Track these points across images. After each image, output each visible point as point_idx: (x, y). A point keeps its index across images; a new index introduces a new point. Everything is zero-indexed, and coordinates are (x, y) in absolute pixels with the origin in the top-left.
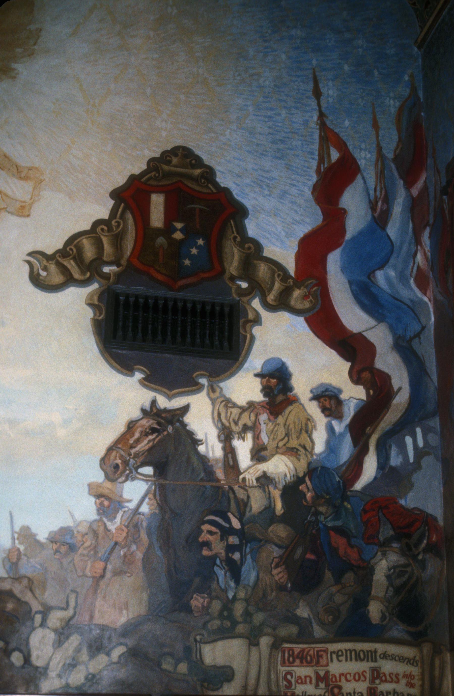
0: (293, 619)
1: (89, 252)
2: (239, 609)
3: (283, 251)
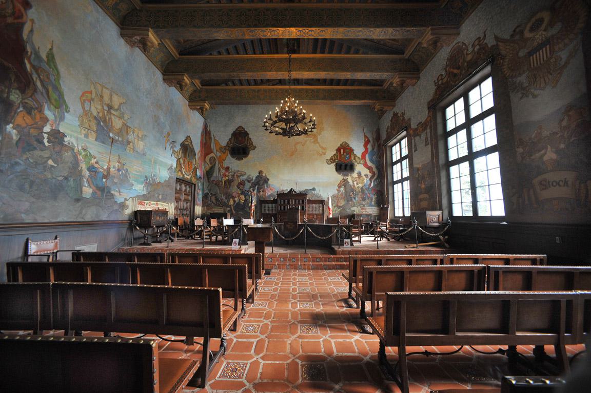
0: (362, 204)
1: (334, 159)
2: (355, 203)
3: (359, 155)
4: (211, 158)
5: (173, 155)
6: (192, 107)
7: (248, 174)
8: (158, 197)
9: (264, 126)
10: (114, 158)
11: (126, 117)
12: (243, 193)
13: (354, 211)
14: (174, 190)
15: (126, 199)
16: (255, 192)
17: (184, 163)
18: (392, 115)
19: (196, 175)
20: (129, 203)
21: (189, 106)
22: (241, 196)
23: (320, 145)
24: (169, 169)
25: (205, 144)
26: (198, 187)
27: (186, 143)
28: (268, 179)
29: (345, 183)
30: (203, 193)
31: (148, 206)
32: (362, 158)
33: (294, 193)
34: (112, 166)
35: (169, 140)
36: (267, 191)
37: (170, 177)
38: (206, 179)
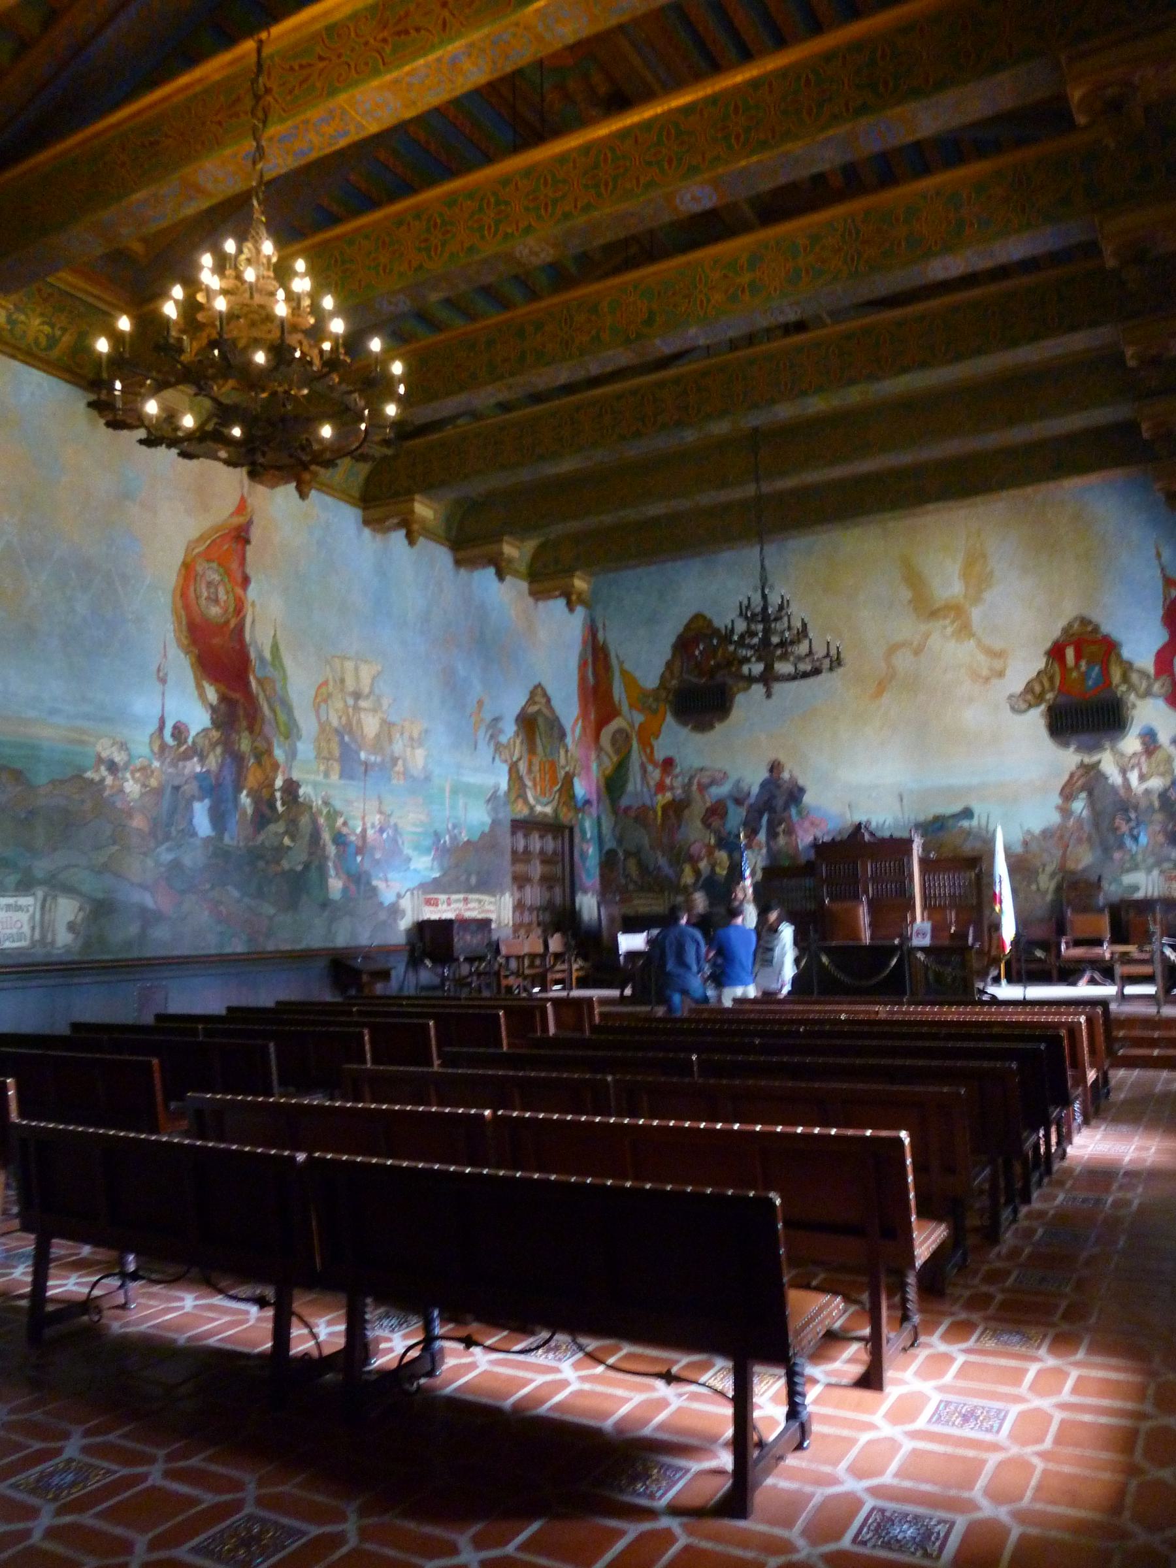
1: (1038, 689)
2: (1140, 857)
7: (733, 777)
8: (468, 879)
10: (373, 805)
11: (385, 702)
13: (1136, 888)
14: (508, 857)
15: (399, 896)
16: (762, 836)
17: (530, 771)
19: (573, 797)
20: (406, 903)
23: (979, 643)
24: (489, 800)
25: (596, 689)
26: (583, 832)
27: (533, 709)
29: (1088, 780)
30: (601, 850)
31: (445, 906)
32: (1158, 673)
34: (369, 825)
35: (482, 720)
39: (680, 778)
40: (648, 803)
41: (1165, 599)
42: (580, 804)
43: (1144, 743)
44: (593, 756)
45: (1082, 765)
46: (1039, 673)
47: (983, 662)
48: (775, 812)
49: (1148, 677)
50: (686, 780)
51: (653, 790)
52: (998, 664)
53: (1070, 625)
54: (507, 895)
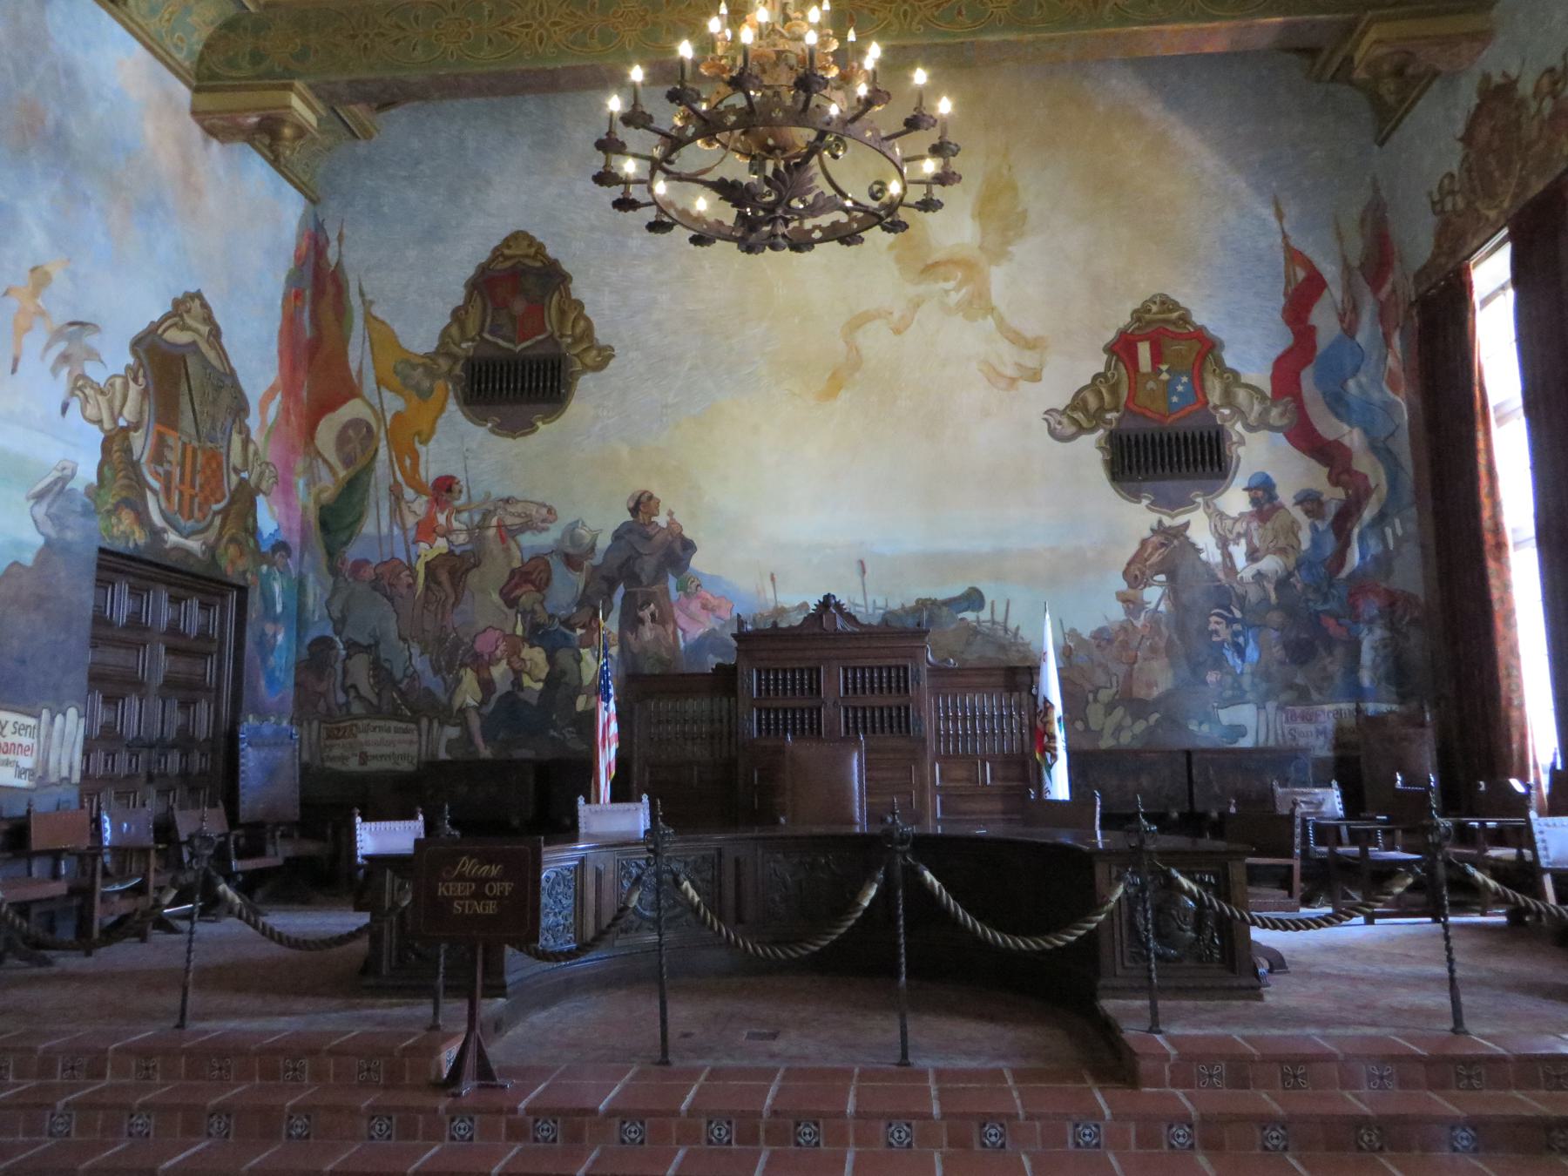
1: (1093, 403)
2: (1246, 681)
4: (345, 427)
5: (75, 405)
6: (217, 128)
7: (566, 517)
9: (605, 178)
12: (537, 634)
17: (158, 458)
18: (1467, 96)
19: (254, 531)
21: (194, 113)
22: (527, 652)
24: (39, 497)
25: (315, 346)
26: (268, 601)
28: (689, 546)
29: (1167, 555)
30: (299, 637)
33: (840, 623)
36: (682, 620)
37: (48, 543)
38: (320, 551)
39: (465, 516)
40: (402, 557)
41: (1288, 283)
42: (265, 548)
43: (1254, 501)
44: (300, 465)
45: (1160, 530)
46: (1096, 377)
47: (1008, 357)
48: (640, 583)
49: (1263, 397)
50: (477, 518)
51: (412, 534)
52: (1030, 359)
53: (1145, 309)
54: (72, 713)
